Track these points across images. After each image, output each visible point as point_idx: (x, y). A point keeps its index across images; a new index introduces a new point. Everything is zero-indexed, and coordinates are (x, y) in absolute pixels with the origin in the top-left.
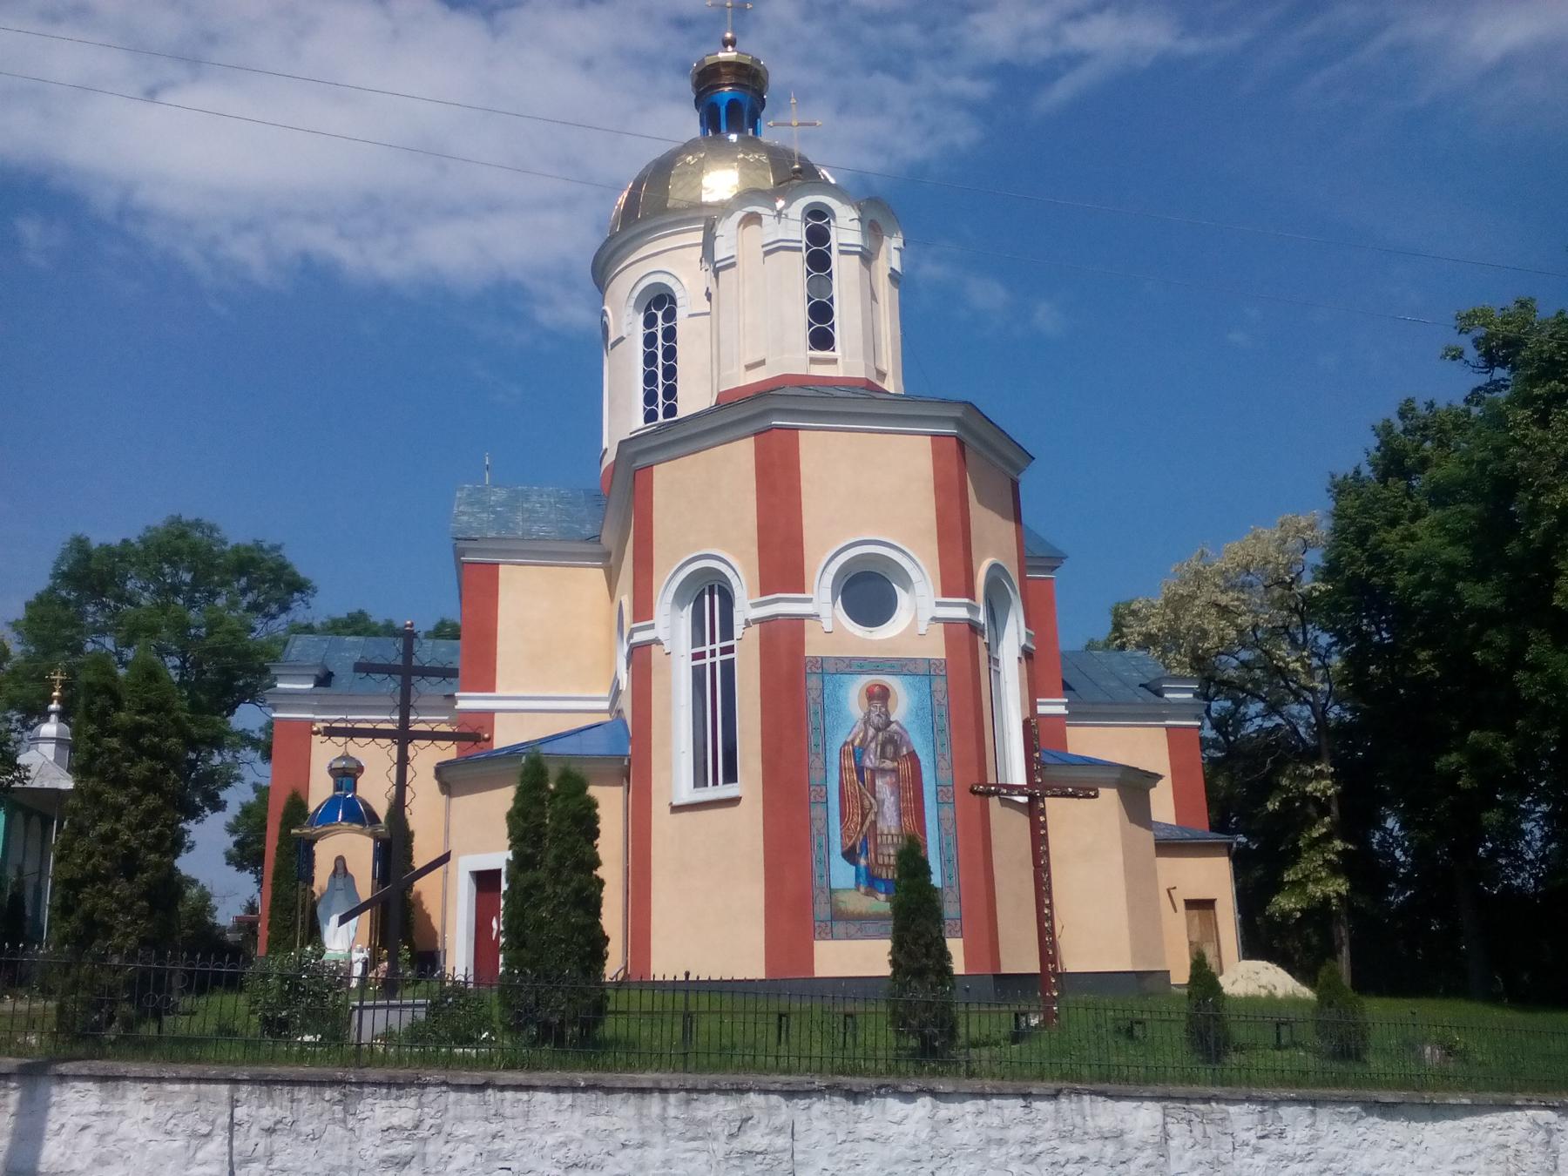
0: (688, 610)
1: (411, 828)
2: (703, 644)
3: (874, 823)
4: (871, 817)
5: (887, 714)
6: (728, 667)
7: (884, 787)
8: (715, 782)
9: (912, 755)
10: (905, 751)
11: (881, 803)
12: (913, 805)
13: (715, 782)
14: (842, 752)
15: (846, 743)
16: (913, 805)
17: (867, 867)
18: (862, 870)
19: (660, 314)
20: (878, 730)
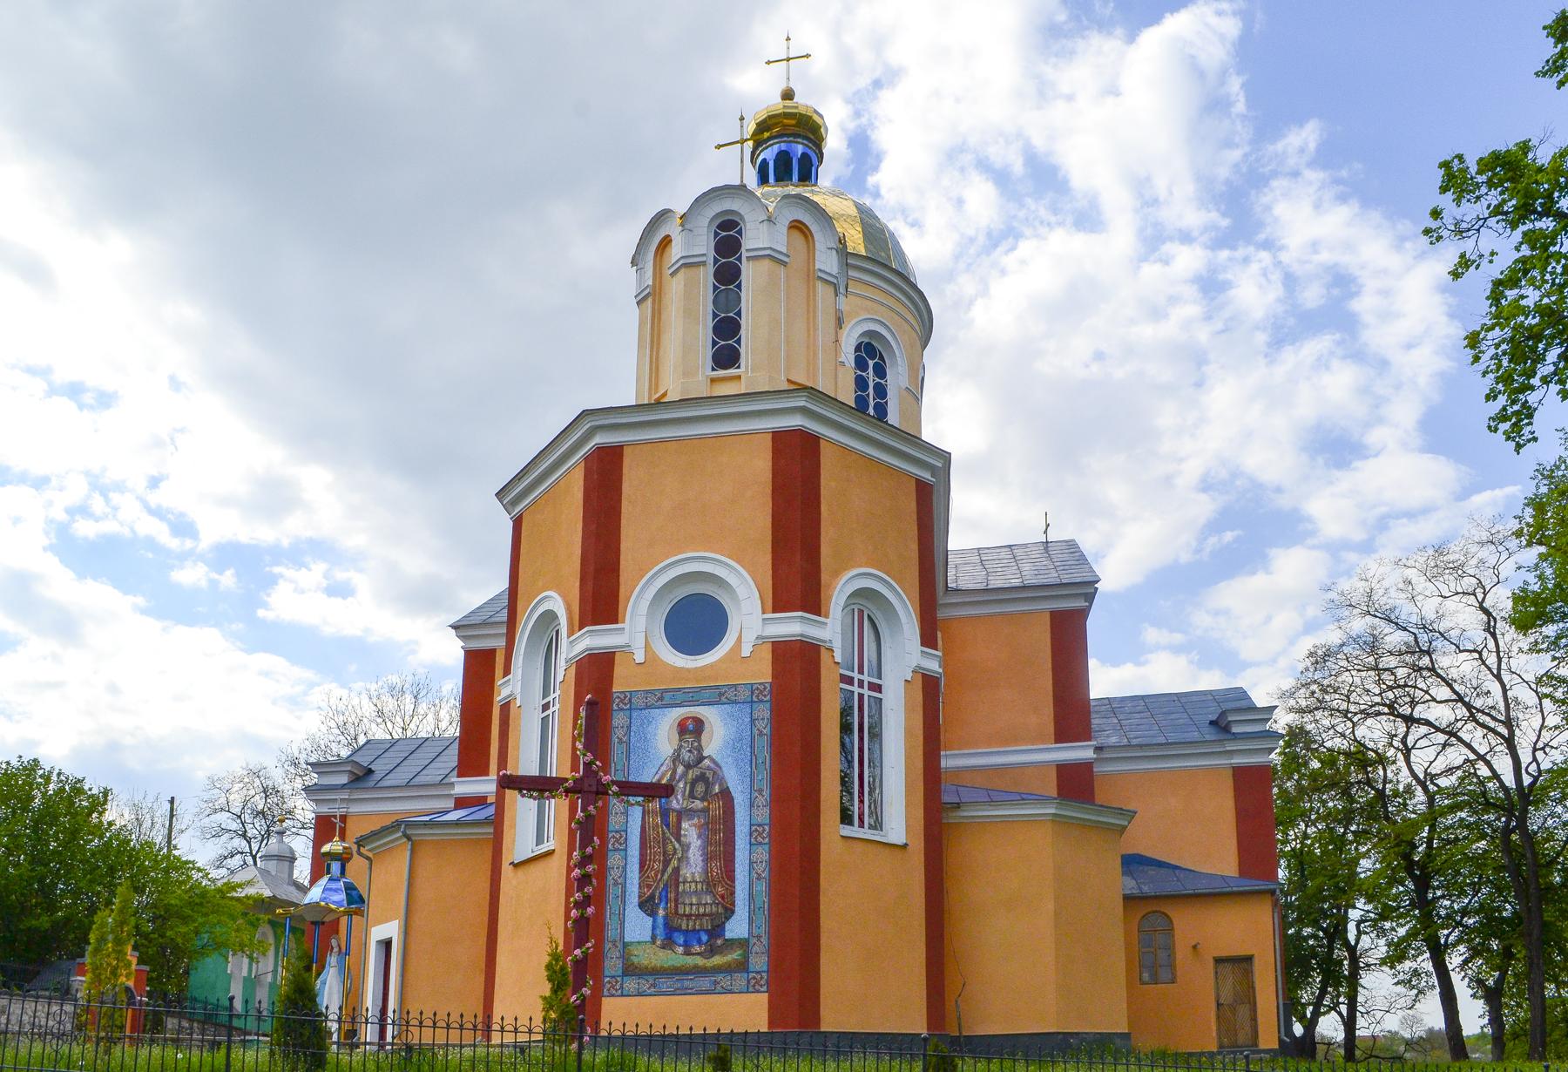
3: (677, 870)
4: (674, 863)
5: (700, 749)
8: (862, 824)
9: (726, 795)
10: (717, 789)
11: (686, 848)
13: (862, 824)
17: (666, 917)
18: (660, 920)
20: (688, 767)
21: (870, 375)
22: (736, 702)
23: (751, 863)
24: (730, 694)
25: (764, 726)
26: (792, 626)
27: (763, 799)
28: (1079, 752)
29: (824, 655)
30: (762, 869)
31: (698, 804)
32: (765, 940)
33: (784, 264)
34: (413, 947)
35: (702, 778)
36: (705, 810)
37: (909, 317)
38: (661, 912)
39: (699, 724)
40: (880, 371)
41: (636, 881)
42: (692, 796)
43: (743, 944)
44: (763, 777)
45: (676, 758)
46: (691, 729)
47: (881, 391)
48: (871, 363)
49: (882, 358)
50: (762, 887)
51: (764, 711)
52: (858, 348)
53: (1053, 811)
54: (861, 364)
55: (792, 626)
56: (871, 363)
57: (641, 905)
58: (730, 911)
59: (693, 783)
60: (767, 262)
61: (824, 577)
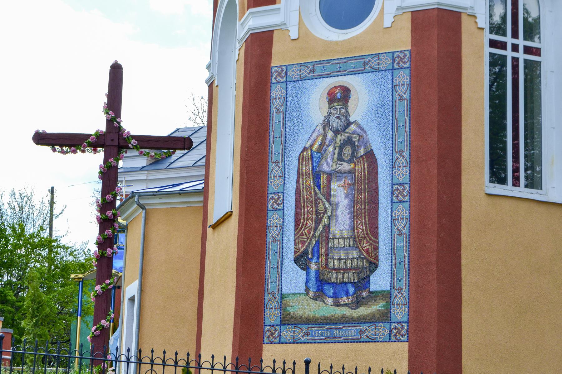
4: (325, 221)
7: (339, 192)
8: (516, 182)
9: (370, 156)
10: (362, 152)
13: (516, 182)
14: (301, 159)
15: (305, 149)
18: (313, 274)
20: (337, 132)
22: (379, 70)
24: (374, 63)
25: (404, 91)
30: (403, 225)
31: (346, 166)
35: (349, 142)
36: (351, 172)
39: (346, 92)
42: (340, 159)
44: (403, 138)
45: (326, 124)
46: (340, 97)
50: (402, 242)
58: (374, 265)
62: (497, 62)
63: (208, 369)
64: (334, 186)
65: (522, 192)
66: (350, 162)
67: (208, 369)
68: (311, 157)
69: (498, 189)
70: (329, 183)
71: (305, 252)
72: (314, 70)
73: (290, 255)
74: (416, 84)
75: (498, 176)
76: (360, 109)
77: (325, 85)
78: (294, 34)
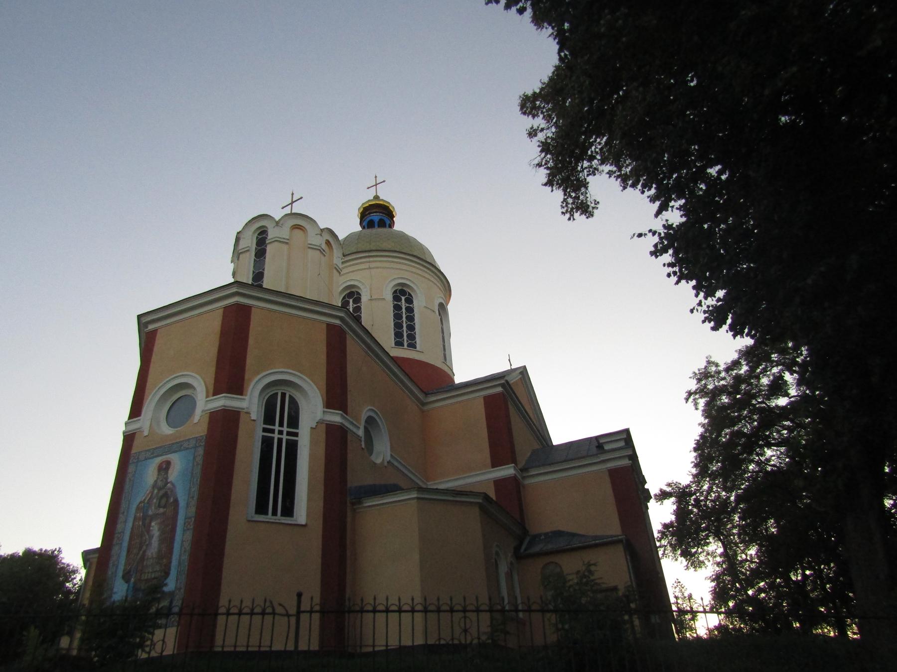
0: (134, 451)
1: (20, 552)
2: (287, 440)
3: (145, 552)
4: (144, 547)
5: (167, 479)
6: (292, 447)
7: (155, 529)
8: (275, 513)
9: (176, 501)
10: (172, 500)
11: (151, 537)
12: (168, 538)
13: (275, 513)
14: (138, 508)
15: (141, 502)
16: (168, 538)
17: (135, 583)
18: (131, 585)
19: (351, 301)
20: (160, 489)
21: (404, 305)
22: (187, 449)
23: (183, 541)
24: (185, 445)
25: (199, 459)
26: (335, 417)
27: (194, 502)
28: (508, 471)
29: (243, 418)
30: (187, 545)
31: (162, 510)
32: (182, 591)
33: (287, 243)
34: (402, 629)
35: (166, 495)
36: (164, 513)
37: (432, 279)
38: (133, 580)
39: (168, 463)
40: (409, 300)
41: (123, 562)
42: (159, 506)
43: (172, 594)
44: (195, 489)
45: (155, 486)
46: (165, 468)
47: (410, 310)
48: (403, 298)
49: (410, 295)
50: (185, 557)
51: (201, 451)
52: (395, 292)
53: (415, 496)
54: (396, 298)
55: (335, 417)
56: (403, 298)
57: (123, 577)
58: (167, 574)
59: (162, 497)
60: (276, 243)
61: (246, 377)
62: (267, 443)
63: (224, 640)
64: (153, 524)
65: (279, 518)
66: (164, 507)
67: (224, 640)
68: (142, 508)
69: (261, 518)
70: (150, 523)
71: (129, 571)
72: (154, 453)
73: (120, 573)
74: (207, 454)
75: (261, 508)
76: (174, 475)
77: (158, 460)
78: (146, 433)
